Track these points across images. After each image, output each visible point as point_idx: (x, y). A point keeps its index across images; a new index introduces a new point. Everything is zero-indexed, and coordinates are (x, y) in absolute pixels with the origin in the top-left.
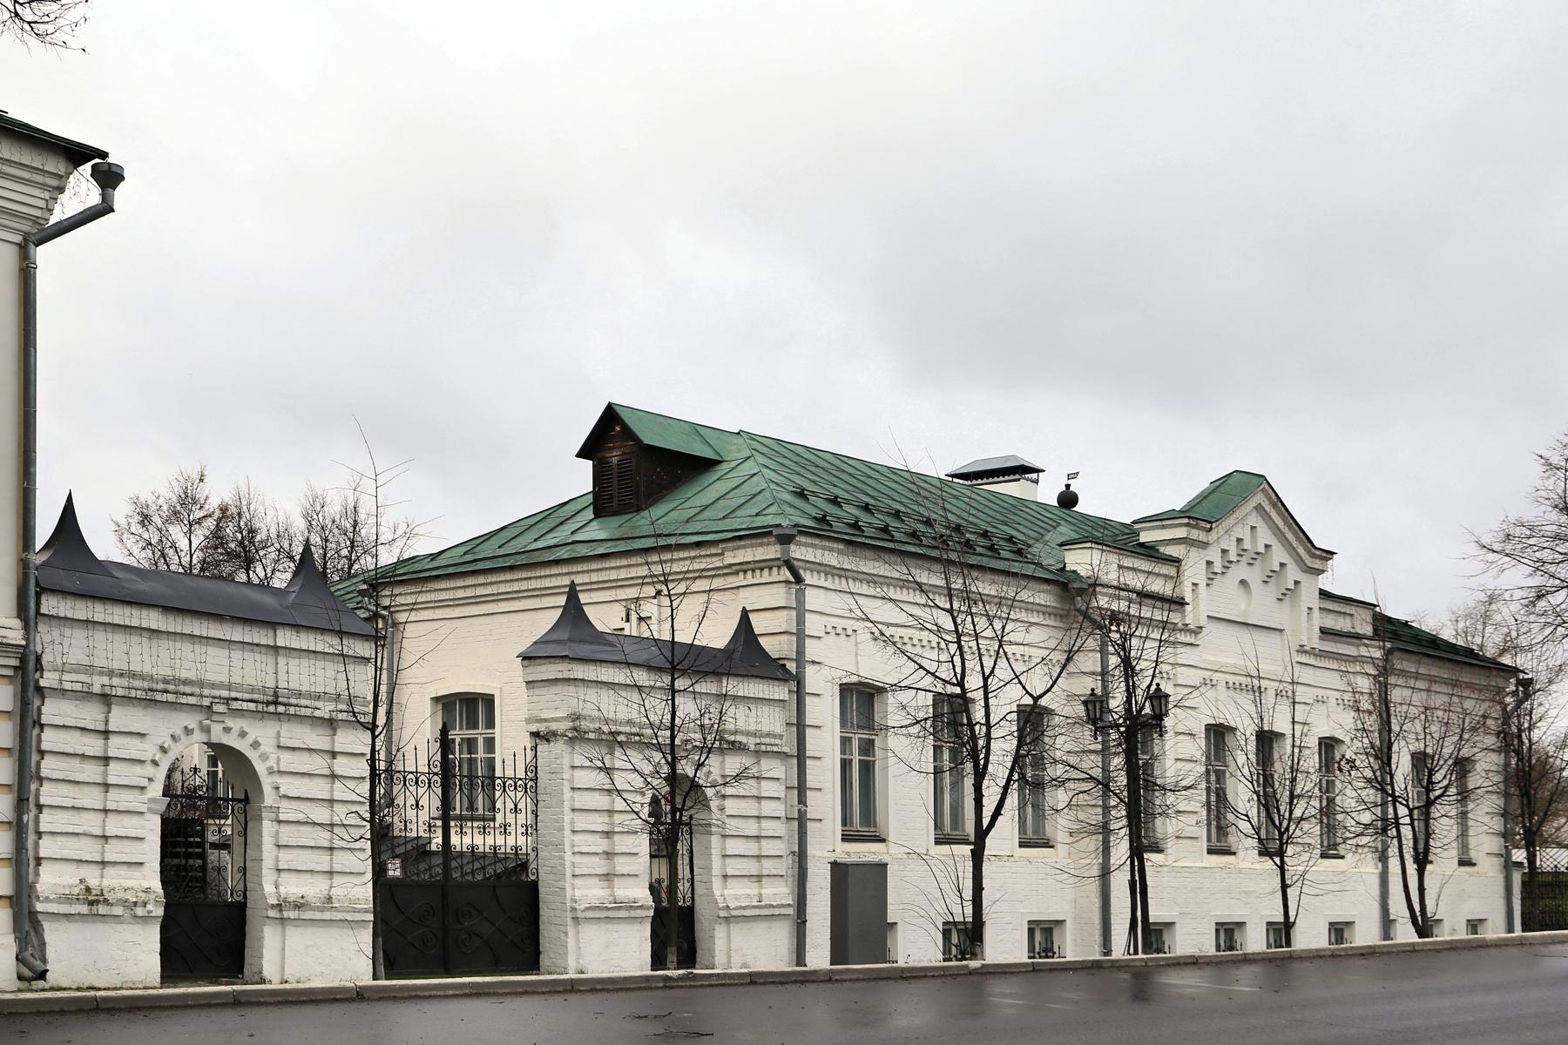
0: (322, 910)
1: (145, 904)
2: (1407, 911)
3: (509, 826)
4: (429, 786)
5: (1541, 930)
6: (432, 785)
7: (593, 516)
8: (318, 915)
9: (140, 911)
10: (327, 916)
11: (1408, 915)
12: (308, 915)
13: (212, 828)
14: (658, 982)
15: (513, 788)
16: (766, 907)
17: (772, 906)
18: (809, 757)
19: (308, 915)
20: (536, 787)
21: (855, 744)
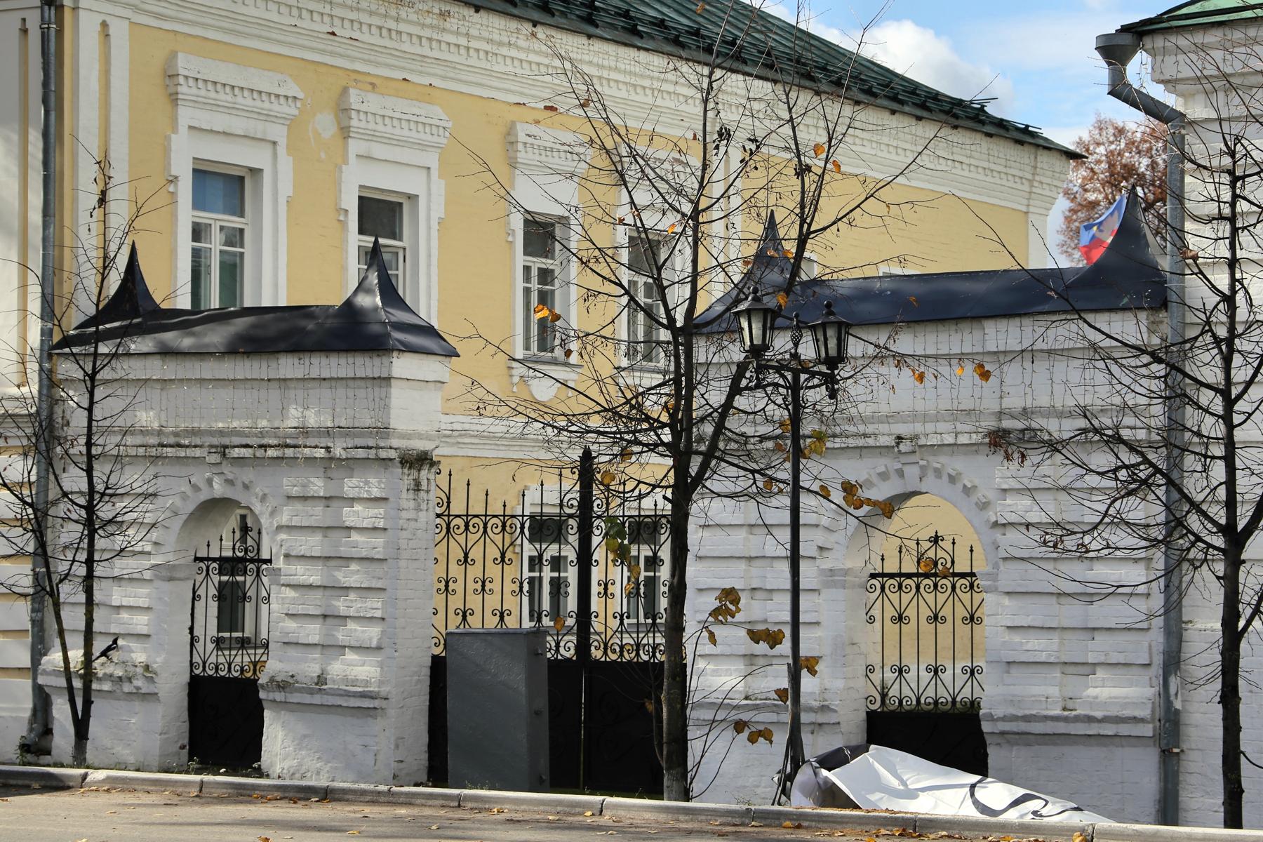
0: (311, 692)
1: (130, 680)
2: (1245, 784)
3: (596, 617)
4: (485, 532)
5: (1137, 822)
6: (489, 530)
7: (755, 342)
8: (307, 699)
9: (127, 688)
10: (317, 699)
11: (30, 171)
12: (295, 698)
13: (596, 643)
14: (452, 801)
15: (500, 529)
16: (1077, 719)
17: (1090, 719)
18: (804, 623)
19: (295, 698)
20: (449, 503)
21: (534, 272)
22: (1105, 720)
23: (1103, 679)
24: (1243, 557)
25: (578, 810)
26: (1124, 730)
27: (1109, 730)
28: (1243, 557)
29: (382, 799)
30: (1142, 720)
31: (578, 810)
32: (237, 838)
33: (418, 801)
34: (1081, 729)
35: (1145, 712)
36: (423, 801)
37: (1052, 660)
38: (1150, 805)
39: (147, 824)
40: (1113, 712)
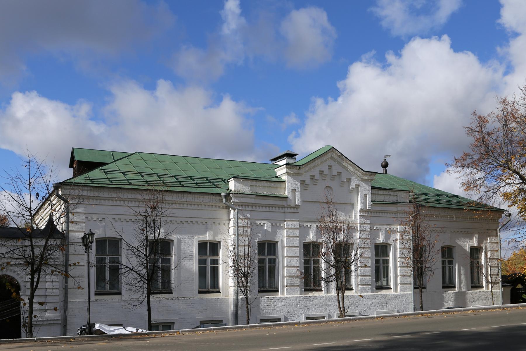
17: (48, 320)
22: (463, 222)
23: (49, 312)
24: (231, 218)
25: (68, 339)
26: (55, 322)
27: (52, 322)
28: (231, 218)
29: (12, 342)
30: (59, 320)
31: (68, 339)
32: (145, 350)
33: (23, 341)
34: (46, 323)
35: (60, 318)
36: (24, 341)
37: (38, 309)
38: (246, 321)
39: (13, 348)
40: (53, 319)
